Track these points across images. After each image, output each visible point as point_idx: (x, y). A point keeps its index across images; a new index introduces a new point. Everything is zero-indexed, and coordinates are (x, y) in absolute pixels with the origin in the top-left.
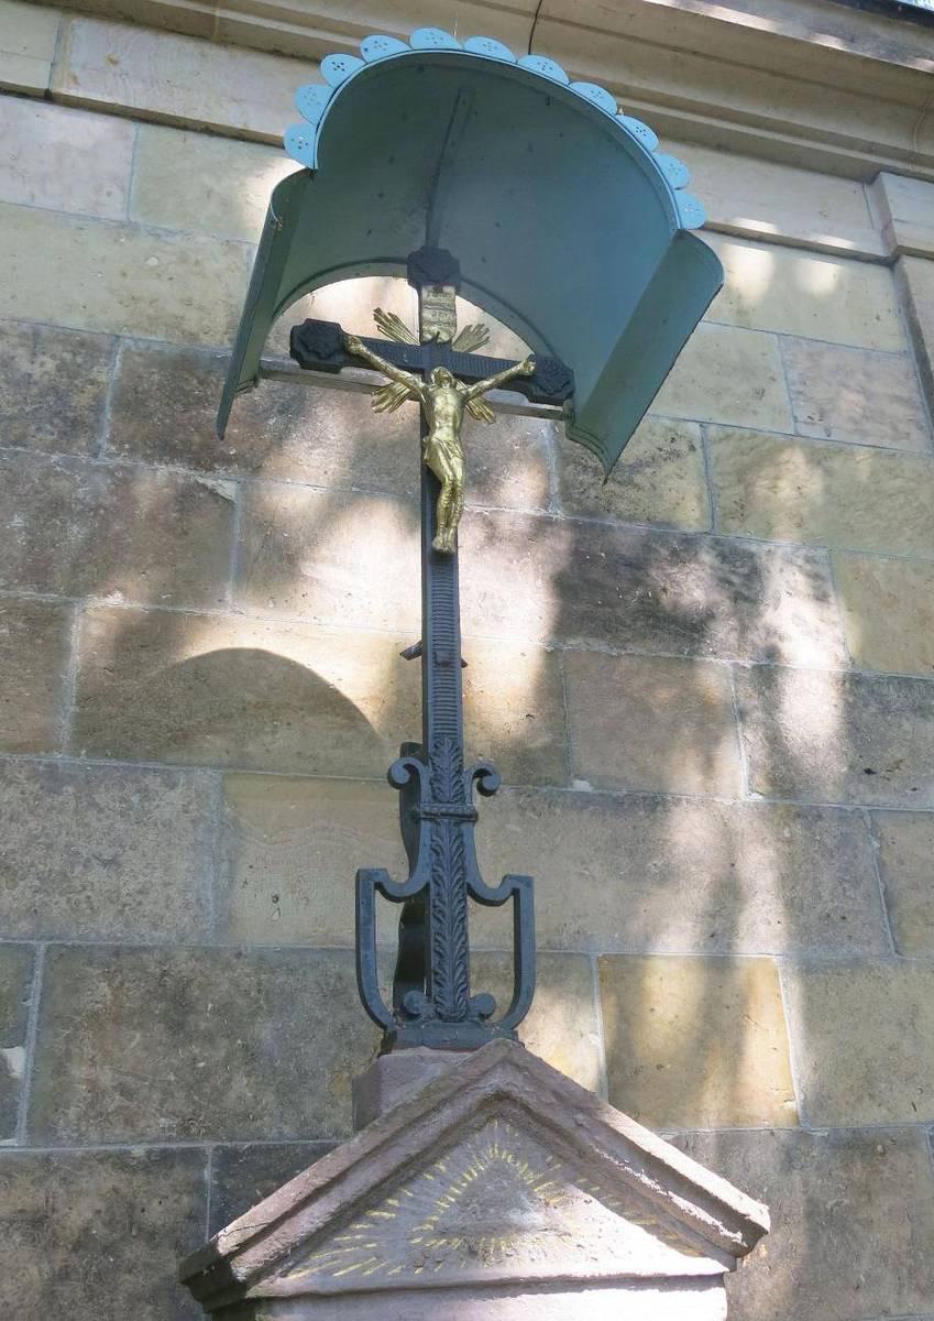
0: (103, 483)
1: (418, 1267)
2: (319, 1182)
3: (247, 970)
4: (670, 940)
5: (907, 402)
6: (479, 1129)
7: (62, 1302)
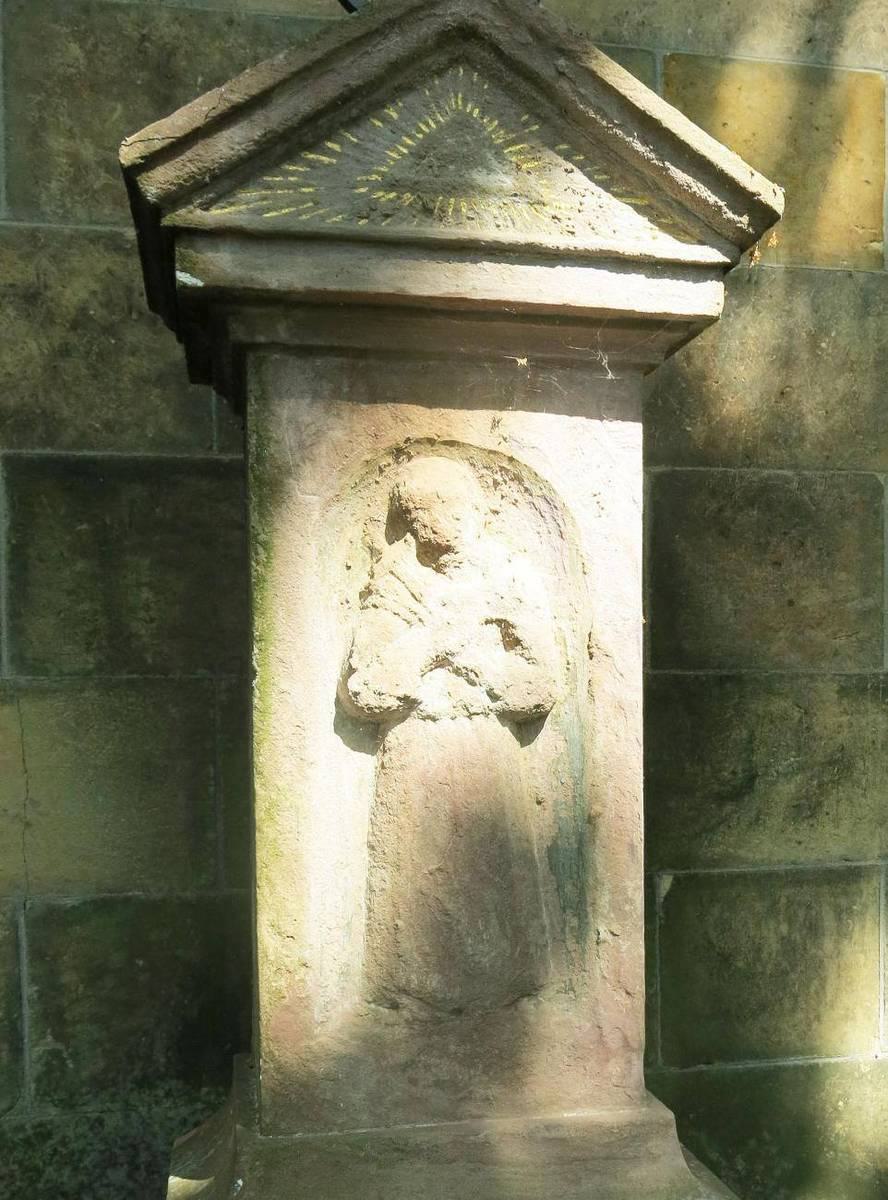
1: (363, 218)
2: (237, 98)
3: (241, 41)
4: (756, 42)
6: (440, 73)
7: (66, 377)
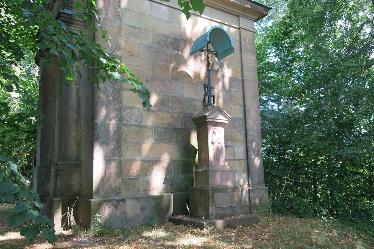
0: (170, 53)
5: (238, 47)
